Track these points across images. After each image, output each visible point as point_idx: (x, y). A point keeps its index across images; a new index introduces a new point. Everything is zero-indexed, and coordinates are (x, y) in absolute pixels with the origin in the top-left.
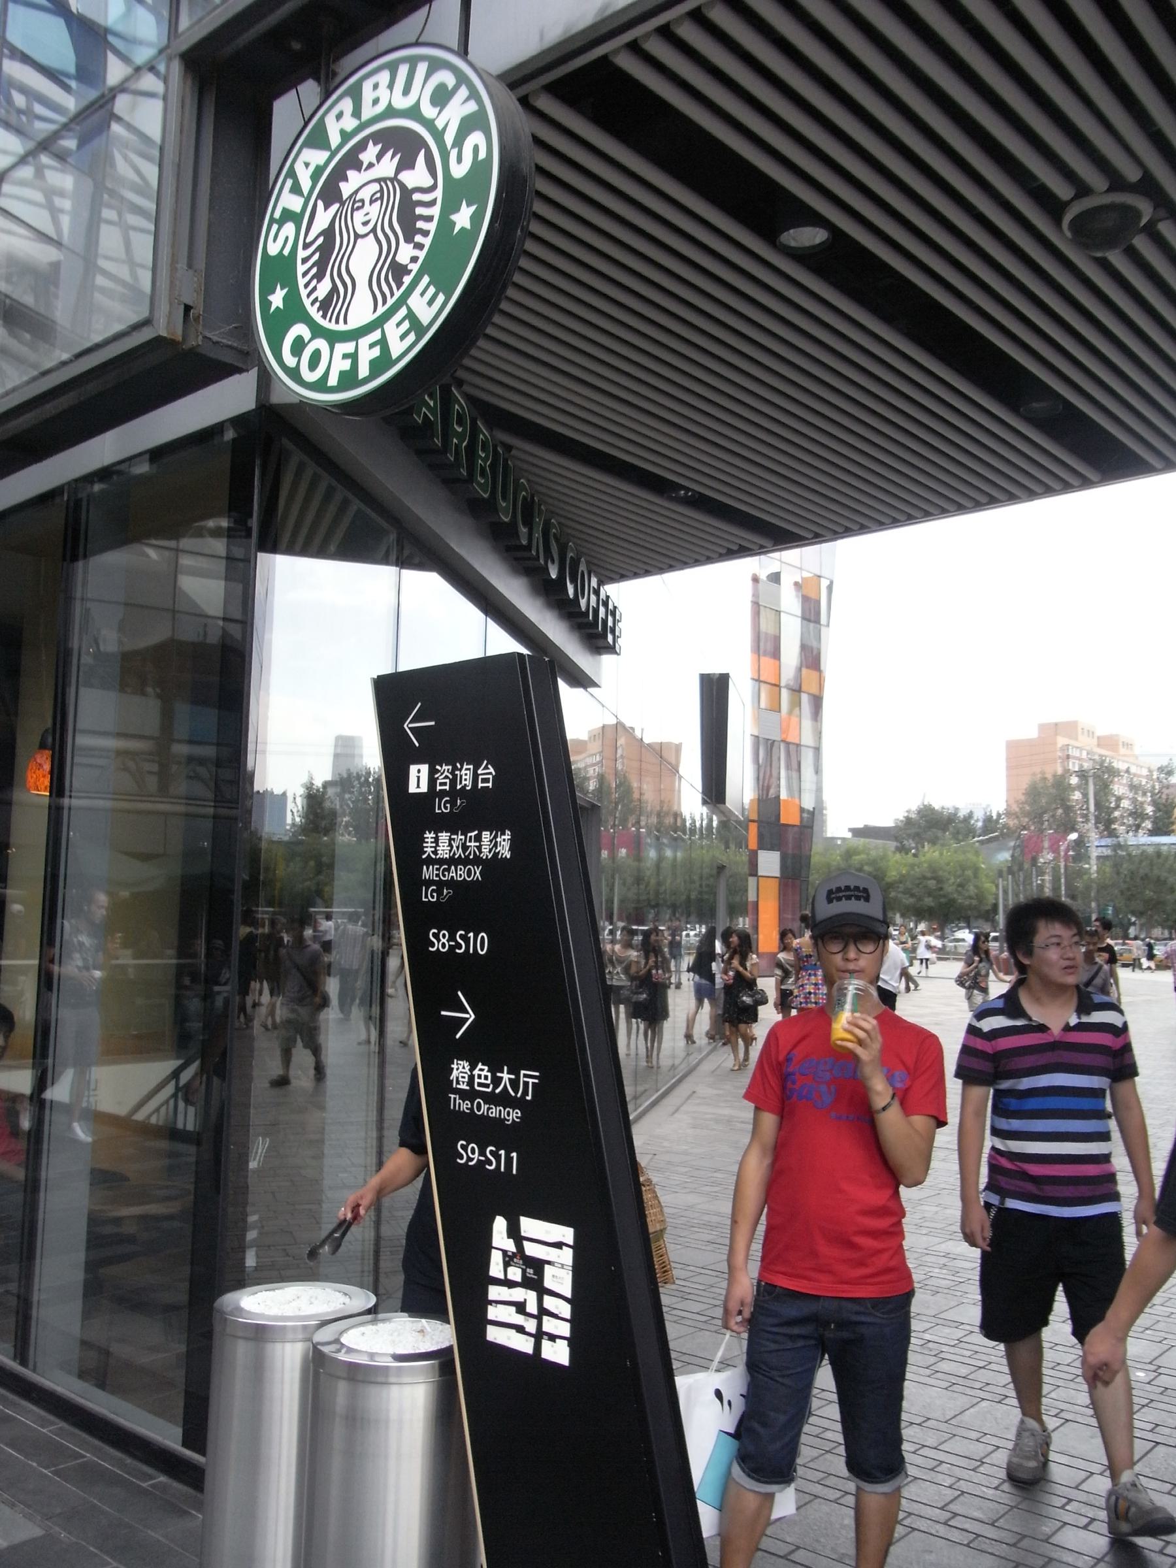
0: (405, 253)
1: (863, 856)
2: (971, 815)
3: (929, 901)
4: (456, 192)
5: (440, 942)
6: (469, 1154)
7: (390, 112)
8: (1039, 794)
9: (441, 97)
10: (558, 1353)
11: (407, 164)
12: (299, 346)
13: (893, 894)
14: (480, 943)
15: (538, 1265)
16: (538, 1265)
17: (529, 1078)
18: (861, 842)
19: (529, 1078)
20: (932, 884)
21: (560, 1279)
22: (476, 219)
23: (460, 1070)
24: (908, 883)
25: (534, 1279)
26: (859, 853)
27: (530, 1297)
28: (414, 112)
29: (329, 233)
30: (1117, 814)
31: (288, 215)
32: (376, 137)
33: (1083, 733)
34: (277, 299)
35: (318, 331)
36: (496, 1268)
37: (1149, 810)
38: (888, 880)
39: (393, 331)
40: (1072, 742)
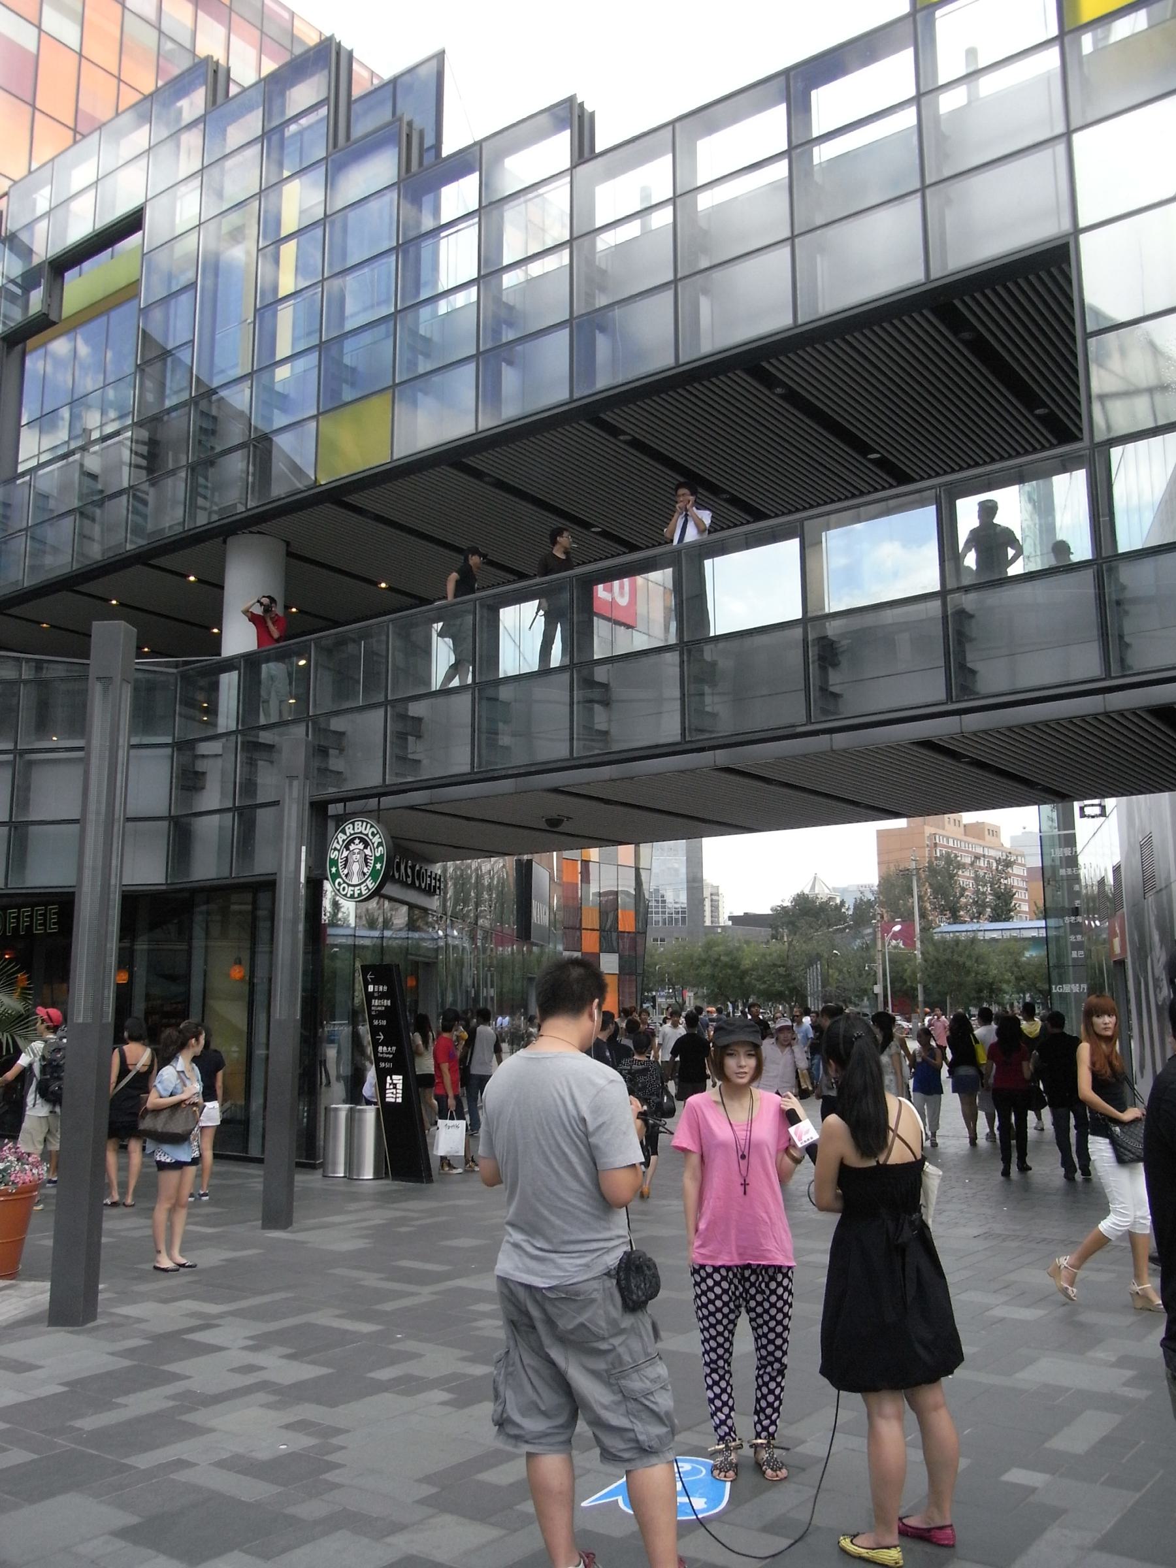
0: (365, 870)
1: (721, 948)
2: (843, 903)
3: (778, 986)
4: (377, 860)
5: (376, 1023)
6: (382, 1065)
7: (361, 833)
8: (893, 885)
9: (373, 834)
10: (399, 1100)
11: (365, 847)
12: (339, 884)
13: (747, 980)
14: (384, 1022)
15: (396, 1084)
16: (396, 1084)
17: (394, 1048)
18: (741, 931)
19: (394, 1048)
20: (781, 970)
21: (400, 1086)
22: (381, 867)
23: (380, 1048)
24: (760, 971)
25: (395, 1088)
26: (718, 946)
27: (394, 1091)
28: (367, 835)
29: (347, 857)
30: (963, 900)
31: (335, 849)
32: (359, 838)
33: (949, 822)
34: (334, 870)
35: (344, 882)
36: (388, 1086)
37: (989, 898)
38: (742, 967)
39: (363, 887)
40: (940, 832)
